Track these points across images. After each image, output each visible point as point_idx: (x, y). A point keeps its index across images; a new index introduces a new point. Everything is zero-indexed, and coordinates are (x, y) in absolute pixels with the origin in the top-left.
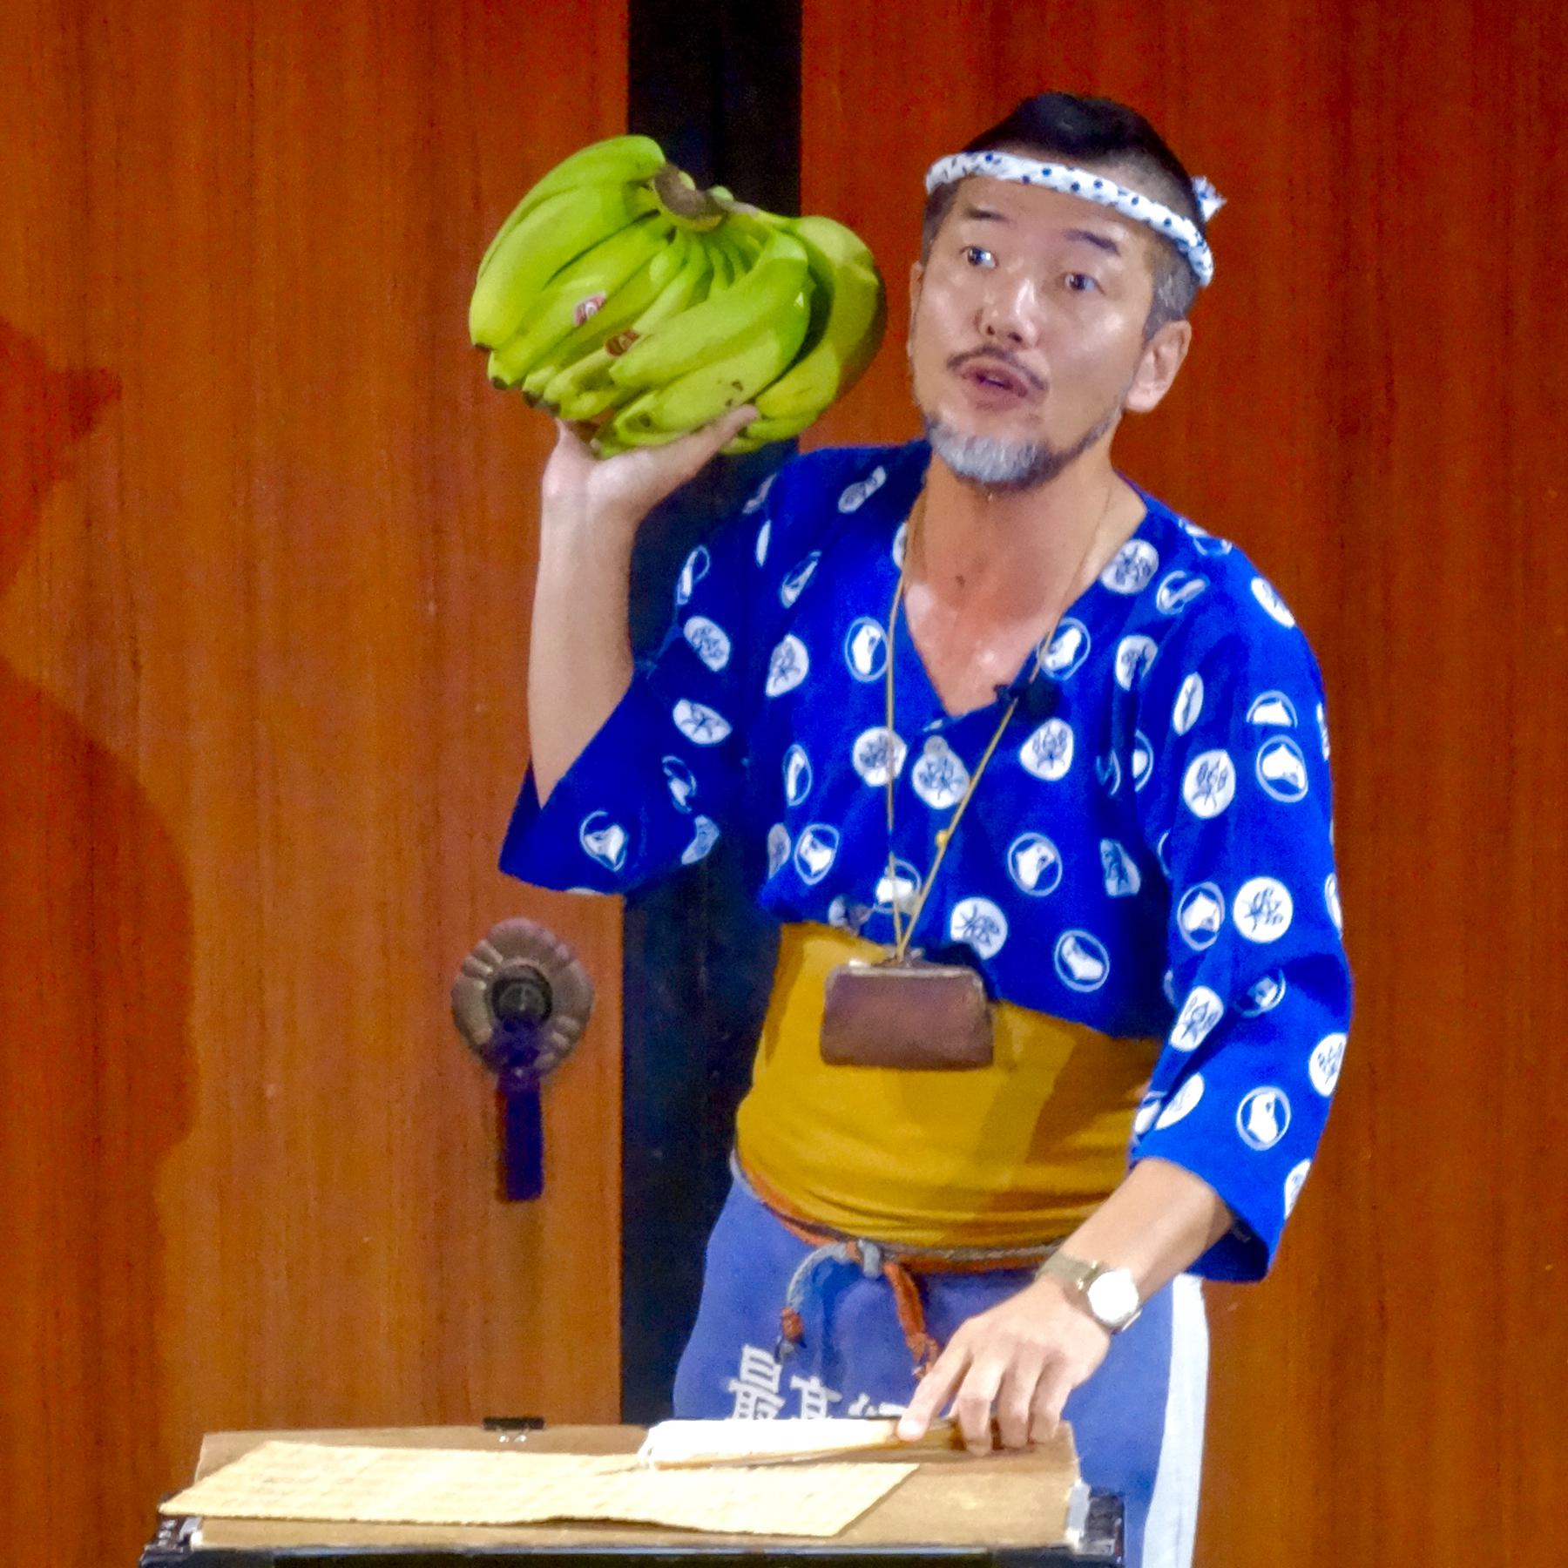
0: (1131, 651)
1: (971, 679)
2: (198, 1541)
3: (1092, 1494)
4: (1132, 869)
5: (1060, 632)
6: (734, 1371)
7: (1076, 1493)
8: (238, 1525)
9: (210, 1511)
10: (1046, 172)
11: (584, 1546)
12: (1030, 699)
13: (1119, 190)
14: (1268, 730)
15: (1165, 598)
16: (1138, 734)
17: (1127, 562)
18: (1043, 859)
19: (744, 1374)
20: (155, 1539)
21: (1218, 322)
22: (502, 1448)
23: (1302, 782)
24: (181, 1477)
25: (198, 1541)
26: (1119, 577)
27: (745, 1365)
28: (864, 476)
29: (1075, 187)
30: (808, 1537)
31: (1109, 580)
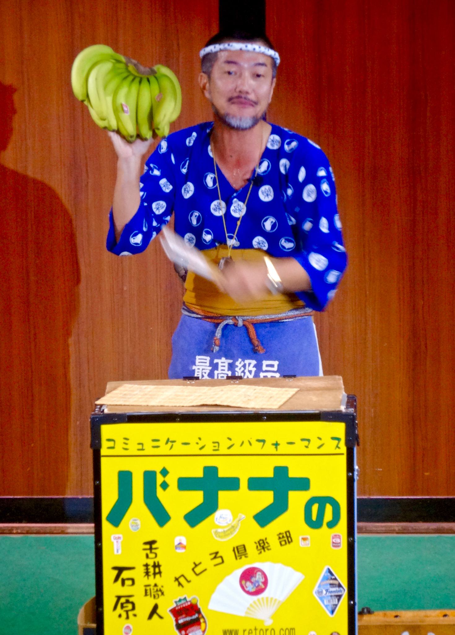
0: (284, 163)
1: (237, 178)
2: (106, 411)
3: (348, 397)
4: (293, 219)
5: (260, 163)
6: (194, 363)
7: (343, 396)
8: (117, 407)
9: (109, 403)
10: (246, 46)
11: (210, 412)
12: (257, 181)
13: (257, 48)
14: (322, 178)
15: (286, 148)
16: (290, 185)
17: (273, 141)
18: (272, 222)
19: (197, 363)
20: (95, 411)
21: (283, 74)
22: (187, 385)
23: (329, 191)
24: (102, 394)
25: (106, 411)
26: (272, 145)
27: (197, 361)
28: (190, 135)
29: (254, 49)
30: (216, 406)
31: (270, 146)
